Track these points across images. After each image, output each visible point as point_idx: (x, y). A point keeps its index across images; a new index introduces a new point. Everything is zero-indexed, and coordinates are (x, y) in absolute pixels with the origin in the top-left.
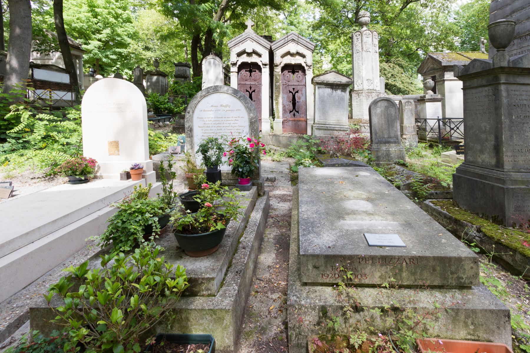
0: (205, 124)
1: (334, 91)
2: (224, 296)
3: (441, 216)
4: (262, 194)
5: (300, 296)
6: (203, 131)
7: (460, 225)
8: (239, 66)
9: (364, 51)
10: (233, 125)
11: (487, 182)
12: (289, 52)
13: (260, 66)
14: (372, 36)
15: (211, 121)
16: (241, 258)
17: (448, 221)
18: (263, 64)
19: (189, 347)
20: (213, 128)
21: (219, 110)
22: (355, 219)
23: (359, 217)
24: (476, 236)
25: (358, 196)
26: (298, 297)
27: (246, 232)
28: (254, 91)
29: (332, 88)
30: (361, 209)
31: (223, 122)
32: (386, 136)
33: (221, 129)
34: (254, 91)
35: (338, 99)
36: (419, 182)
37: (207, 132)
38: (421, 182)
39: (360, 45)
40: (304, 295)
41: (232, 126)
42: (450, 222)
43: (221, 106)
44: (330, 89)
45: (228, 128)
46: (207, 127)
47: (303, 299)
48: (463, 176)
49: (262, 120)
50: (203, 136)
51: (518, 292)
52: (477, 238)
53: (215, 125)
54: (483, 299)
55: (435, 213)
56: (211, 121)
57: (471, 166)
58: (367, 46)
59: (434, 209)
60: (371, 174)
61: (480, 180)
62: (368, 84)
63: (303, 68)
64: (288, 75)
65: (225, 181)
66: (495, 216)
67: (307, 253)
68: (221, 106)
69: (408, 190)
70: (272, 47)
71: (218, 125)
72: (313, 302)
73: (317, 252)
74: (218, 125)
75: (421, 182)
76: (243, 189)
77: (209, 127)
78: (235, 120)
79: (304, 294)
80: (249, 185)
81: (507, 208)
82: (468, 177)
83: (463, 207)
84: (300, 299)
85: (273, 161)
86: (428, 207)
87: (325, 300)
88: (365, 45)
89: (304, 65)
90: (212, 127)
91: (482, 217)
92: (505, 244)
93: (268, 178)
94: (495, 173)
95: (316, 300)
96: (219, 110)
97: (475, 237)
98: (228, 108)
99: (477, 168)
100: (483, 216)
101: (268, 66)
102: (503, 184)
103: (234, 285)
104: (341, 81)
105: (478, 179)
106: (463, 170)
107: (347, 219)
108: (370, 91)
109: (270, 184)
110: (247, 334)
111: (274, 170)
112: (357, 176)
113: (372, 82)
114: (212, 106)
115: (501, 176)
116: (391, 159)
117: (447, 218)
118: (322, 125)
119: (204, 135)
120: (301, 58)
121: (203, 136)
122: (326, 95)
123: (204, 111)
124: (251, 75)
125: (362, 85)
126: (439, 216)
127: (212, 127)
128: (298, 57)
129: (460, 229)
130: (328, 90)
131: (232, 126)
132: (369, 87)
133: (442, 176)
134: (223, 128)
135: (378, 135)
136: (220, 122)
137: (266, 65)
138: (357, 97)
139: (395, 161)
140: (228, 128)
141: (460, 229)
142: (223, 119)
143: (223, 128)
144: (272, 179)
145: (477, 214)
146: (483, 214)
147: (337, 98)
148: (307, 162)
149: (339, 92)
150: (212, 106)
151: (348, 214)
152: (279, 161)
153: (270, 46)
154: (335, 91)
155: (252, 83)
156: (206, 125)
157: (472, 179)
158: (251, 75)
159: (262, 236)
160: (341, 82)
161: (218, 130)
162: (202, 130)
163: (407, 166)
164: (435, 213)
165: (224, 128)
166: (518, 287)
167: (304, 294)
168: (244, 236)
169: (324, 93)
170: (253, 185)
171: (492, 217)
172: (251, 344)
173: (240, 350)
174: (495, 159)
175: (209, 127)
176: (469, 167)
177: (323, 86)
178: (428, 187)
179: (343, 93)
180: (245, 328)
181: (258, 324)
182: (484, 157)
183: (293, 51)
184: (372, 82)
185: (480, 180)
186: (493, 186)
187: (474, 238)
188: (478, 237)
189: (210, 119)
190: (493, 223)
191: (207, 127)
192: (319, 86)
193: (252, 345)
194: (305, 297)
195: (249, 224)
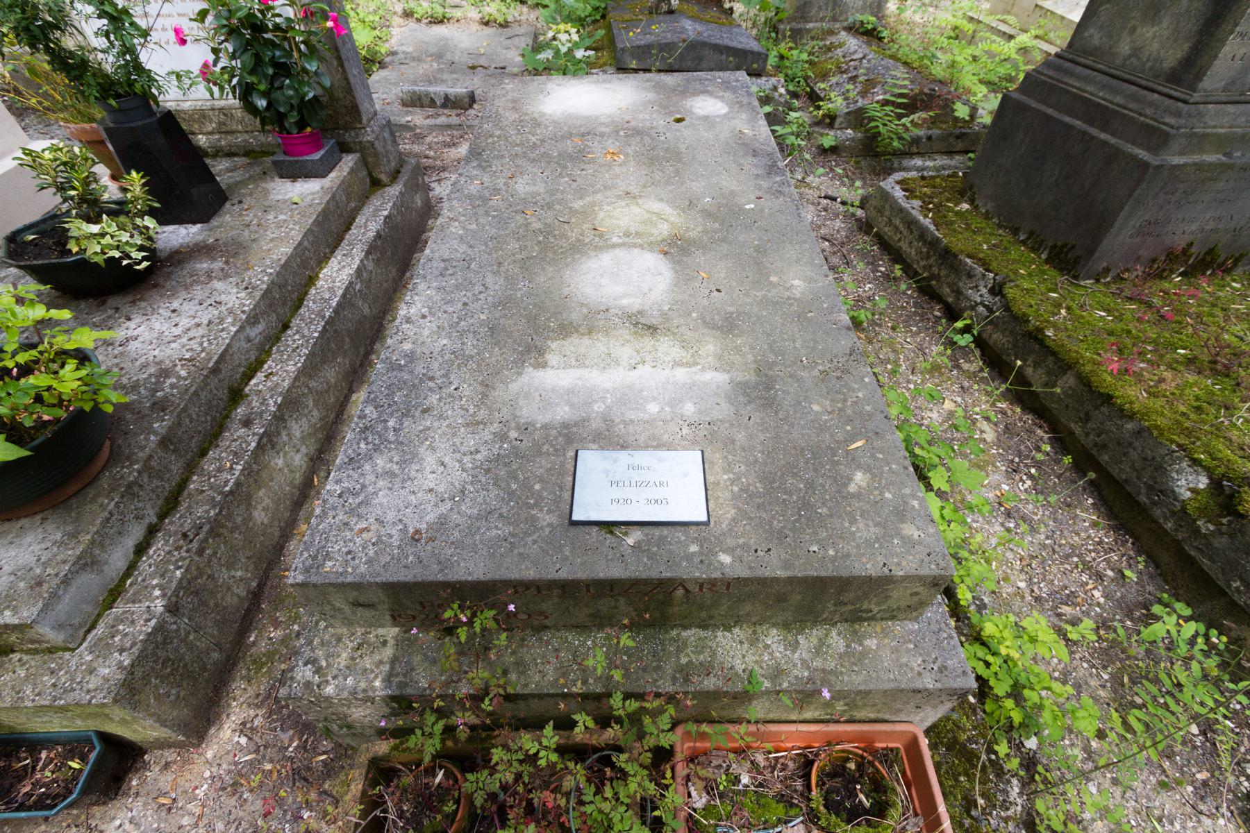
2: (101, 650)
3: (912, 233)
5: (329, 665)
7: (952, 267)
11: (1103, 136)
16: (220, 470)
17: (925, 250)
19: (44, 755)
22: (580, 361)
23: (599, 345)
24: (982, 303)
25: (641, 229)
26: (318, 671)
27: (278, 351)
30: (625, 302)
36: (893, 103)
38: (899, 106)
40: (343, 659)
42: (928, 253)
47: (334, 678)
48: (1034, 104)
51: (1017, 460)
52: (981, 309)
54: (908, 650)
55: (897, 222)
57: (1079, 69)
59: (901, 210)
60: (731, 105)
61: (1085, 127)
65: (246, 136)
66: (1064, 246)
67: (314, 579)
69: (854, 128)
72: (363, 685)
73: (360, 569)
75: (899, 106)
76: (295, 173)
79: (344, 655)
80: (317, 156)
81: (1114, 230)
82: (1050, 111)
83: (985, 205)
84: (325, 675)
85: (487, 24)
86: (886, 200)
87: (405, 675)
91: (1024, 243)
92: (1051, 344)
93: (447, 97)
94: (1151, 104)
95: (376, 677)
97: (977, 304)
99: (1100, 77)
100: (1028, 238)
102: (1154, 150)
103: (157, 593)
105: (1078, 123)
106: (1043, 83)
107: (552, 359)
109: (455, 120)
110: (255, 662)
111: (483, 62)
112: (679, 121)
115: (1167, 120)
116: (841, 14)
117: (925, 241)
126: (905, 232)
129: (947, 276)
133: (968, 79)
139: (851, 20)
141: (947, 276)
144: (461, 100)
145: (1015, 231)
146: (1031, 234)
148: (564, 37)
151: (566, 330)
152: (505, 25)
157: (1059, 121)
159: (383, 318)
163: (881, 39)
164: (897, 222)
166: (1022, 447)
167: (344, 655)
168: (266, 366)
170: (345, 148)
171: (1054, 247)
172: (258, 695)
173: (224, 716)
174: (1186, 46)
176: (1072, 74)
178: (912, 122)
180: (254, 643)
181: (296, 627)
182: (1150, 35)
185: (1085, 127)
186: (1118, 152)
187: (973, 308)
188: (985, 306)
190: (1047, 261)
193: (260, 698)
194: (341, 666)
195: (302, 311)
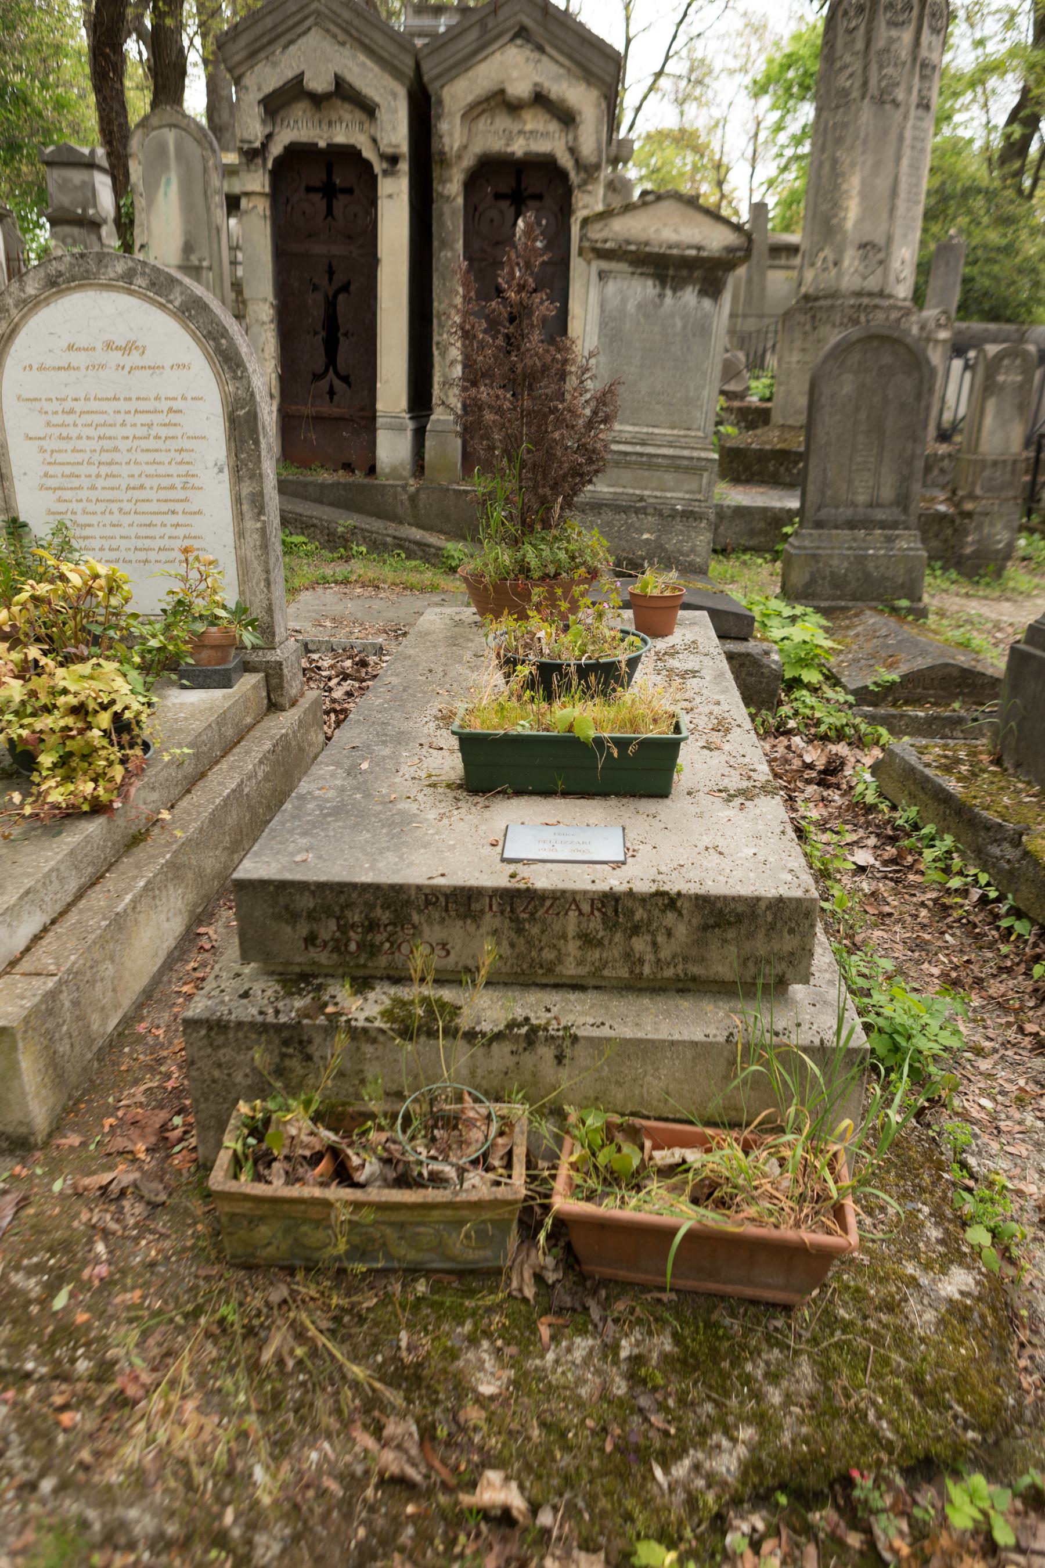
0: (48, 424)
1: (669, 292)
4: (286, 702)
6: (47, 455)
8: (279, 161)
9: (867, 100)
10: (164, 432)
12: (502, 92)
13: (368, 165)
14: (921, 18)
15: (72, 411)
18: (383, 157)
20: (83, 444)
21: (102, 366)
28: (345, 288)
29: (662, 279)
31: (119, 418)
32: (862, 498)
33: (116, 449)
34: (345, 288)
35: (684, 328)
37: (60, 457)
39: (857, 66)
41: (157, 437)
43: (109, 346)
44: (650, 283)
45: (144, 444)
46: (61, 437)
49: (380, 421)
50: (46, 475)
53: (90, 431)
56: (72, 411)
58: (889, 71)
62: (861, 268)
63: (562, 175)
64: (494, 214)
68: (109, 346)
70: (425, 66)
71: (102, 431)
74: (102, 431)
77: (68, 438)
78: (170, 410)
88: (881, 67)
89: (565, 161)
90: (79, 438)
96: (102, 366)
98: (135, 359)
101: (404, 166)
104: (704, 243)
108: (865, 301)
113: (881, 256)
114: (71, 347)
118: (628, 448)
119: (52, 470)
120: (554, 126)
121: (46, 475)
122: (631, 307)
123: (40, 369)
124: (330, 212)
125: (834, 272)
127: (79, 438)
128: (534, 121)
130: (643, 289)
131: (157, 437)
132: (866, 284)
134: (123, 445)
135: (829, 493)
136: (109, 419)
137: (393, 160)
138: (808, 327)
140: (144, 444)
142: (122, 405)
143: (123, 445)
147: (679, 324)
149: (689, 296)
150: (71, 347)
153: (410, 62)
154: (675, 290)
155: (338, 250)
156: (56, 431)
158: (330, 212)
160: (699, 248)
161: (103, 450)
162: (42, 450)
165: (128, 443)
169: (624, 301)
175: (68, 438)
177: (623, 266)
179: (707, 303)
183: (520, 89)
184: (881, 256)
189: (69, 405)
191: (61, 437)
192: (605, 265)
